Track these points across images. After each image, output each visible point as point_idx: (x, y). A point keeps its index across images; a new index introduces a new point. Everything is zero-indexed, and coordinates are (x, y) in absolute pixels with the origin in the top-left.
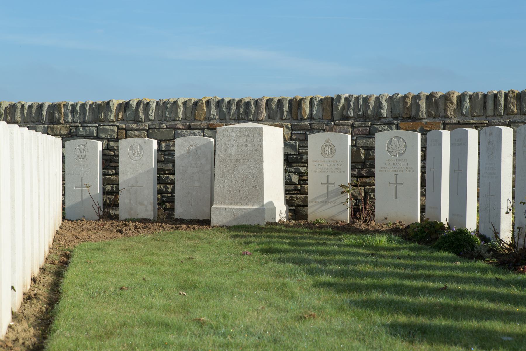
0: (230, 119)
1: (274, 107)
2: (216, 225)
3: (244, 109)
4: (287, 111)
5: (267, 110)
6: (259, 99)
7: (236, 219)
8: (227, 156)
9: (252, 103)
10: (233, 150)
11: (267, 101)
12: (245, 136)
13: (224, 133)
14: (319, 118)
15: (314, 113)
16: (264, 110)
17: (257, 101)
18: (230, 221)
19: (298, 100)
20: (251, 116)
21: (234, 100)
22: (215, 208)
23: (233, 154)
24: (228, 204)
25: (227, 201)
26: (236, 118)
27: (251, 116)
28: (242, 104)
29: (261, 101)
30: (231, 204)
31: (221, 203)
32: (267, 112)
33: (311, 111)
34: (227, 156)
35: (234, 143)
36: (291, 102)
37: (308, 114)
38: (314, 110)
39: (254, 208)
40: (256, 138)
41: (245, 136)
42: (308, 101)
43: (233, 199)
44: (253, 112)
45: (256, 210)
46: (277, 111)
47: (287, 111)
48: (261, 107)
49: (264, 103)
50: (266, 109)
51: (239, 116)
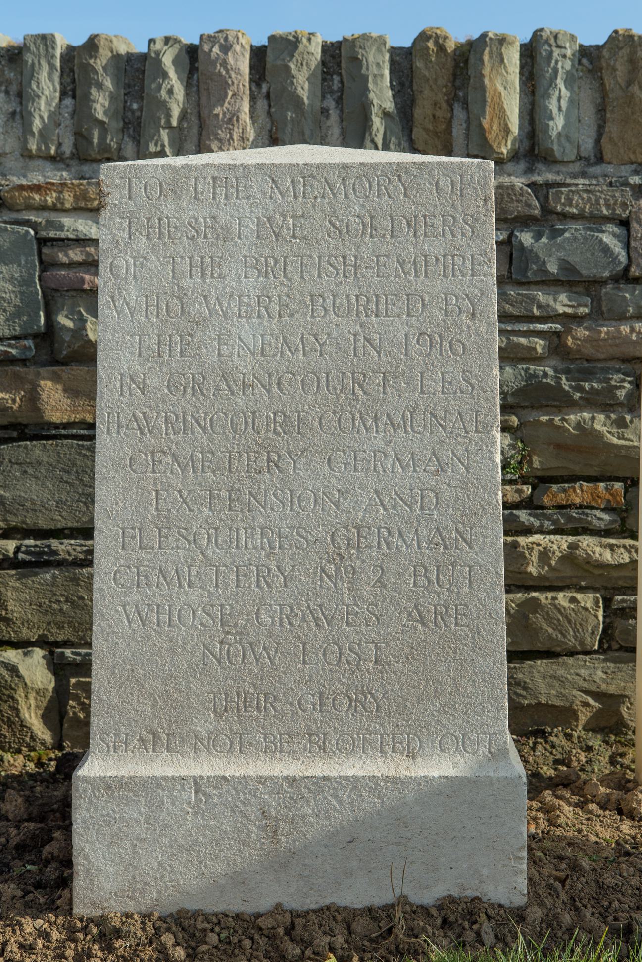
0: (27, 155)
1: (303, 84)
2: (115, 909)
3: (113, 98)
4: (386, 114)
5: (262, 104)
6: (211, 39)
7: (281, 863)
8: (197, 388)
9: (167, 60)
10: (245, 340)
11: (258, 54)
12: (340, 231)
13: (168, 208)
14: (580, 158)
15: (558, 123)
16: (246, 107)
17: (192, 53)
18: (238, 880)
19: (451, 46)
20: (164, 135)
21: (46, 40)
22: (109, 785)
23: (244, 367)
24: (211, 744)
25: (201, 726)
26: (67, 149)
27: (164, 135)
28: (99, 63)
29: (226, 48)
30: (241, 746)
31: (152, 741)
32: (263, 118)
33: (533, 114)
34: (197, 388)
35: (253, 284)
36: (403, 62)
37: (515, 128)
38: (553, 106)
39: (434, 772)
40: (436, 248)
41: (340, 231)
42: (513, 57)
43: (246, 714)
44: (176, 112)
45: (454, 785)
46: (324, 111)
47: (386, 114)
48: (224, 85)
49: (244, 65)
50: (253, 99)
51: (81, 137)
